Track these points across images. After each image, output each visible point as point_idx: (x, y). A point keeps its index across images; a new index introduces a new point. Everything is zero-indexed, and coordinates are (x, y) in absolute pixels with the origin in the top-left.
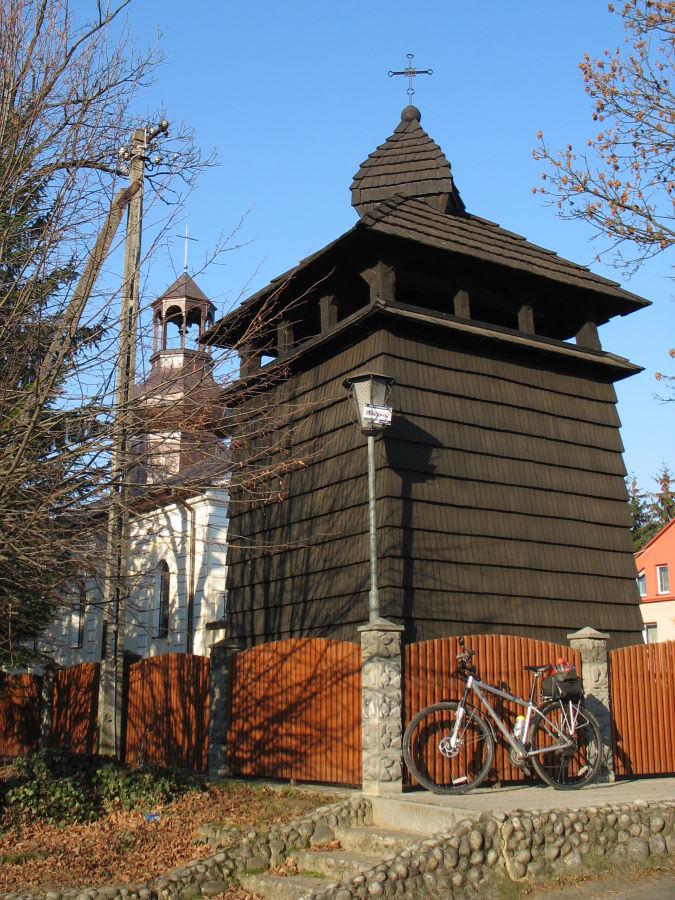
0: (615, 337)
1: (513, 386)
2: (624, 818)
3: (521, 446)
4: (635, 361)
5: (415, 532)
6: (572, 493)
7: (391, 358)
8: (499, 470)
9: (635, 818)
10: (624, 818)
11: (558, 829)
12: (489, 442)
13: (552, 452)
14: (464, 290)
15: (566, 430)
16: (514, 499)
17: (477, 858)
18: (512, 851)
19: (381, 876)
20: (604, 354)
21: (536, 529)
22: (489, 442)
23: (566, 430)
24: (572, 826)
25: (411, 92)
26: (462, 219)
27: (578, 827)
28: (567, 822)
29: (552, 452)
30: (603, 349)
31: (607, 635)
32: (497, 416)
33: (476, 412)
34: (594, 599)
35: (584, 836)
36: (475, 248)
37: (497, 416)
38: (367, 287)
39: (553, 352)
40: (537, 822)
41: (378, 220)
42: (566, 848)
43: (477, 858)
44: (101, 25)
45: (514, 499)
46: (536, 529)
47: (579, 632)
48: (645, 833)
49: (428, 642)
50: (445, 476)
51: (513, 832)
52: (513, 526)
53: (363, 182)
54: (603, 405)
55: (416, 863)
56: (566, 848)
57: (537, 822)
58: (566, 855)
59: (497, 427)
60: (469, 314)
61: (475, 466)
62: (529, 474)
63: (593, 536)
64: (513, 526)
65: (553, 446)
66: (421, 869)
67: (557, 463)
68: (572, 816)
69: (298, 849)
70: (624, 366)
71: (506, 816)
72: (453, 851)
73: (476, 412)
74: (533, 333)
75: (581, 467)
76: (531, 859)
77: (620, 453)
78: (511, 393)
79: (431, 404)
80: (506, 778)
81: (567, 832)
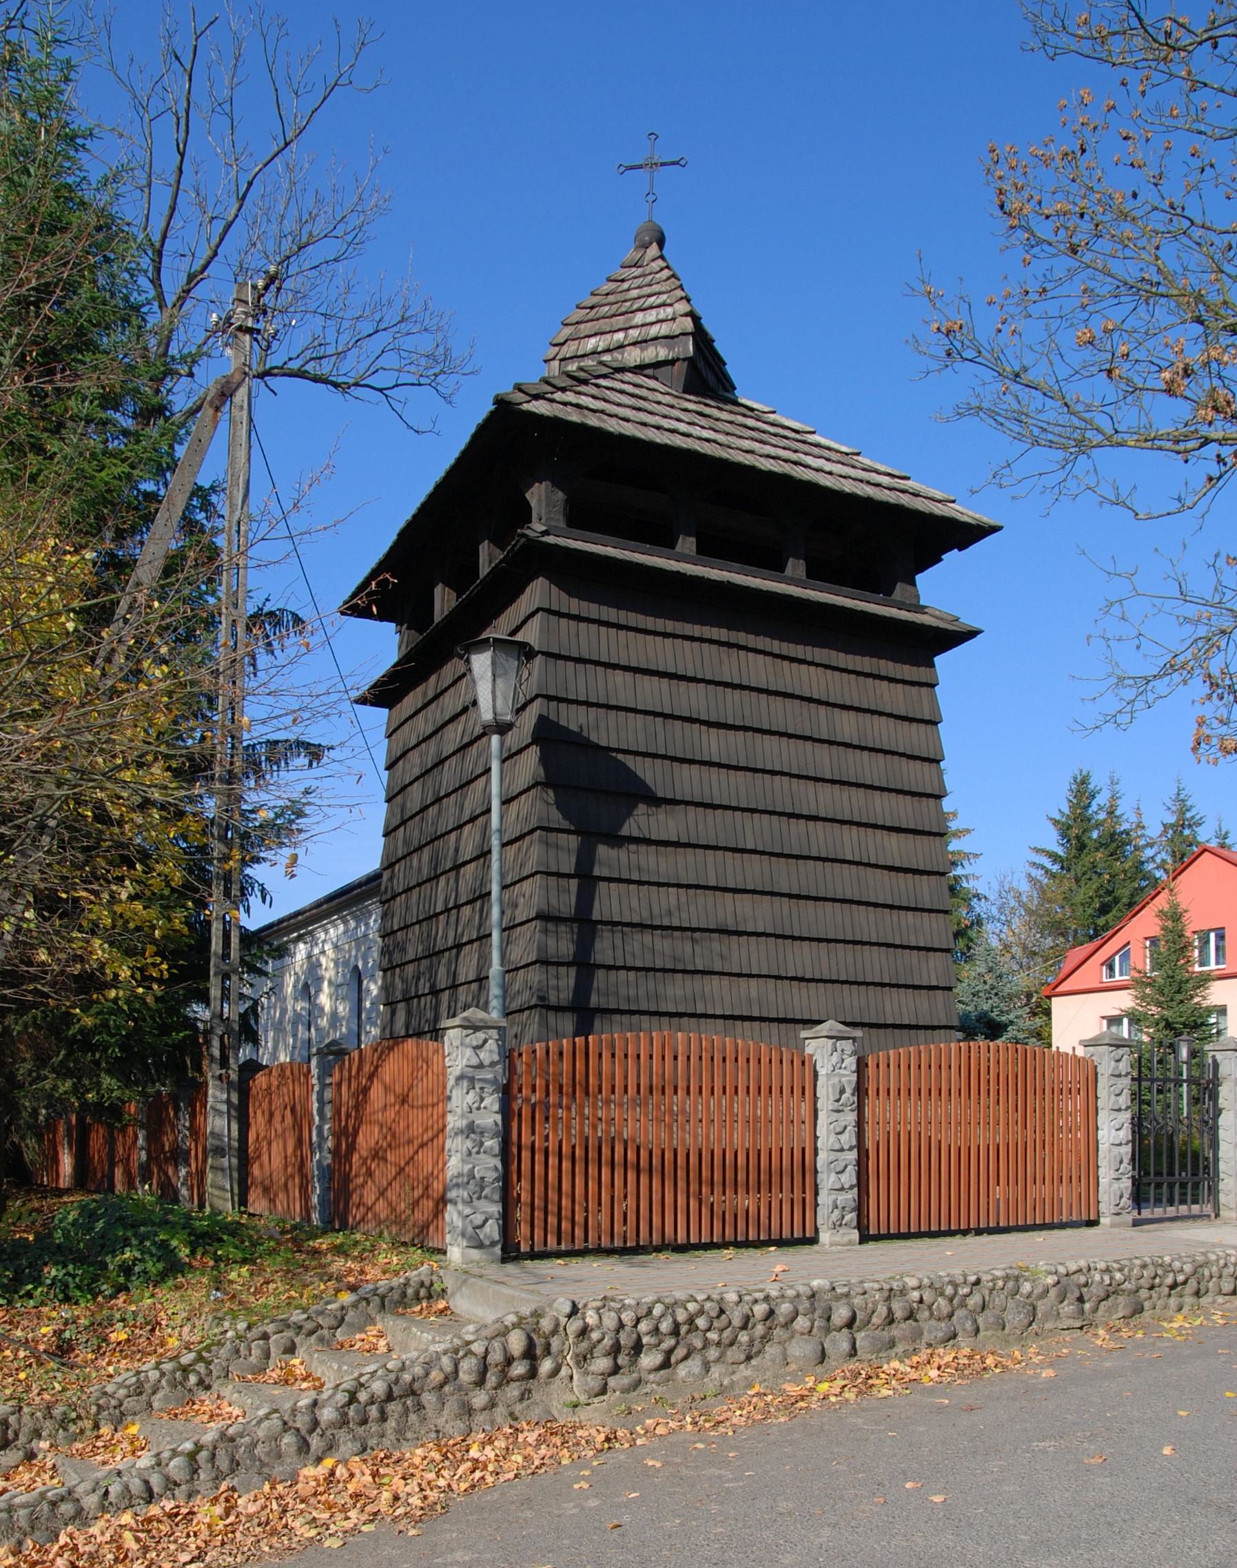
0: (941, 589)
1: (816, 673)
2: (785, 1308)
3: (770, 751)
4: (969, 620)
5: (602, 885)
6: (851, 823)
7: (554, 619)
8: (720, 785)
9: (804, 1305)
10: (785, 1308)
11: (665, 1326)
12: (714, 744)
13: (823, 760)
14: (557, 484)
15: (847, 726)
16: (753, 831)
17: (519, 1369)
18: (583, 1359)
19: (341, 1398)
20: (921, 609)
21: (786, 876)
22: (714, 744)
23: (847, 726)
24: (691, 1321)
25: (651, 198)
26: (708, 402)
27: (701, 1322)
28: (681, 1316)
29: (823, 760)
30: (922, 603)
31: (858, 1033)
32: (731, 705)
33: (694, 699)
34: (878, 980)
35: (712, 1336)
36: (708, 440)
37: (731, 705)
38: (529, 509)
39: (826, 604)
40: (627, 1317)
41: (537, 397)
42: (680, 1352)
43: (519, 1369)
44: (287, 144)
45: (753, 831)
46: (786, 876)
47: (819, 1027)
48: (820, 1328)
49: (901, 1050)
50: (673, 802)
51: (584, 1332)
52: (753, 871)
53: (565, 348)
54: (915, 689)
55: (407, 1377)
56: (680, 1352)
57: (627, 1317)
58: (677, 1363)
59: (730, 722)
60: (694, 548)
61: (688, 781)
62: (781, 792)
63: (880, 886)
64: (753, 871)
65: (822, 751)
66: (416, 1386)
67: (828, 776)
68: (692, 1307)
69: (950, 1282)
70: (950, 627)
71: (574, 1305)
72: (474, 1361)
73: (694, 699)
74: (694, 553)
75: (868, 782)
76: (616, 1370)
77: (938, 762)
78: (758, 670)
79: (581, 682)
80: (739, 1239)
81: (683, 1329)
